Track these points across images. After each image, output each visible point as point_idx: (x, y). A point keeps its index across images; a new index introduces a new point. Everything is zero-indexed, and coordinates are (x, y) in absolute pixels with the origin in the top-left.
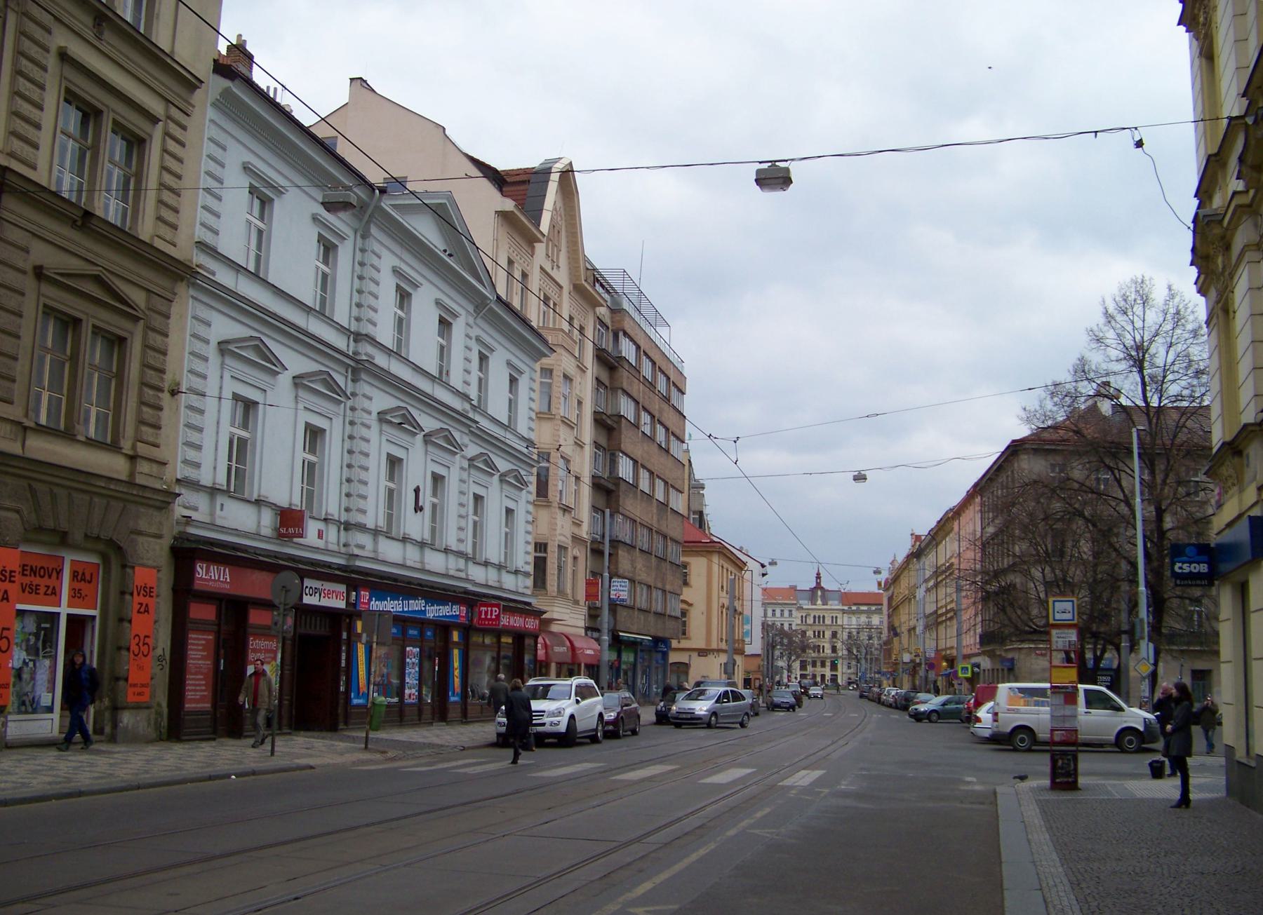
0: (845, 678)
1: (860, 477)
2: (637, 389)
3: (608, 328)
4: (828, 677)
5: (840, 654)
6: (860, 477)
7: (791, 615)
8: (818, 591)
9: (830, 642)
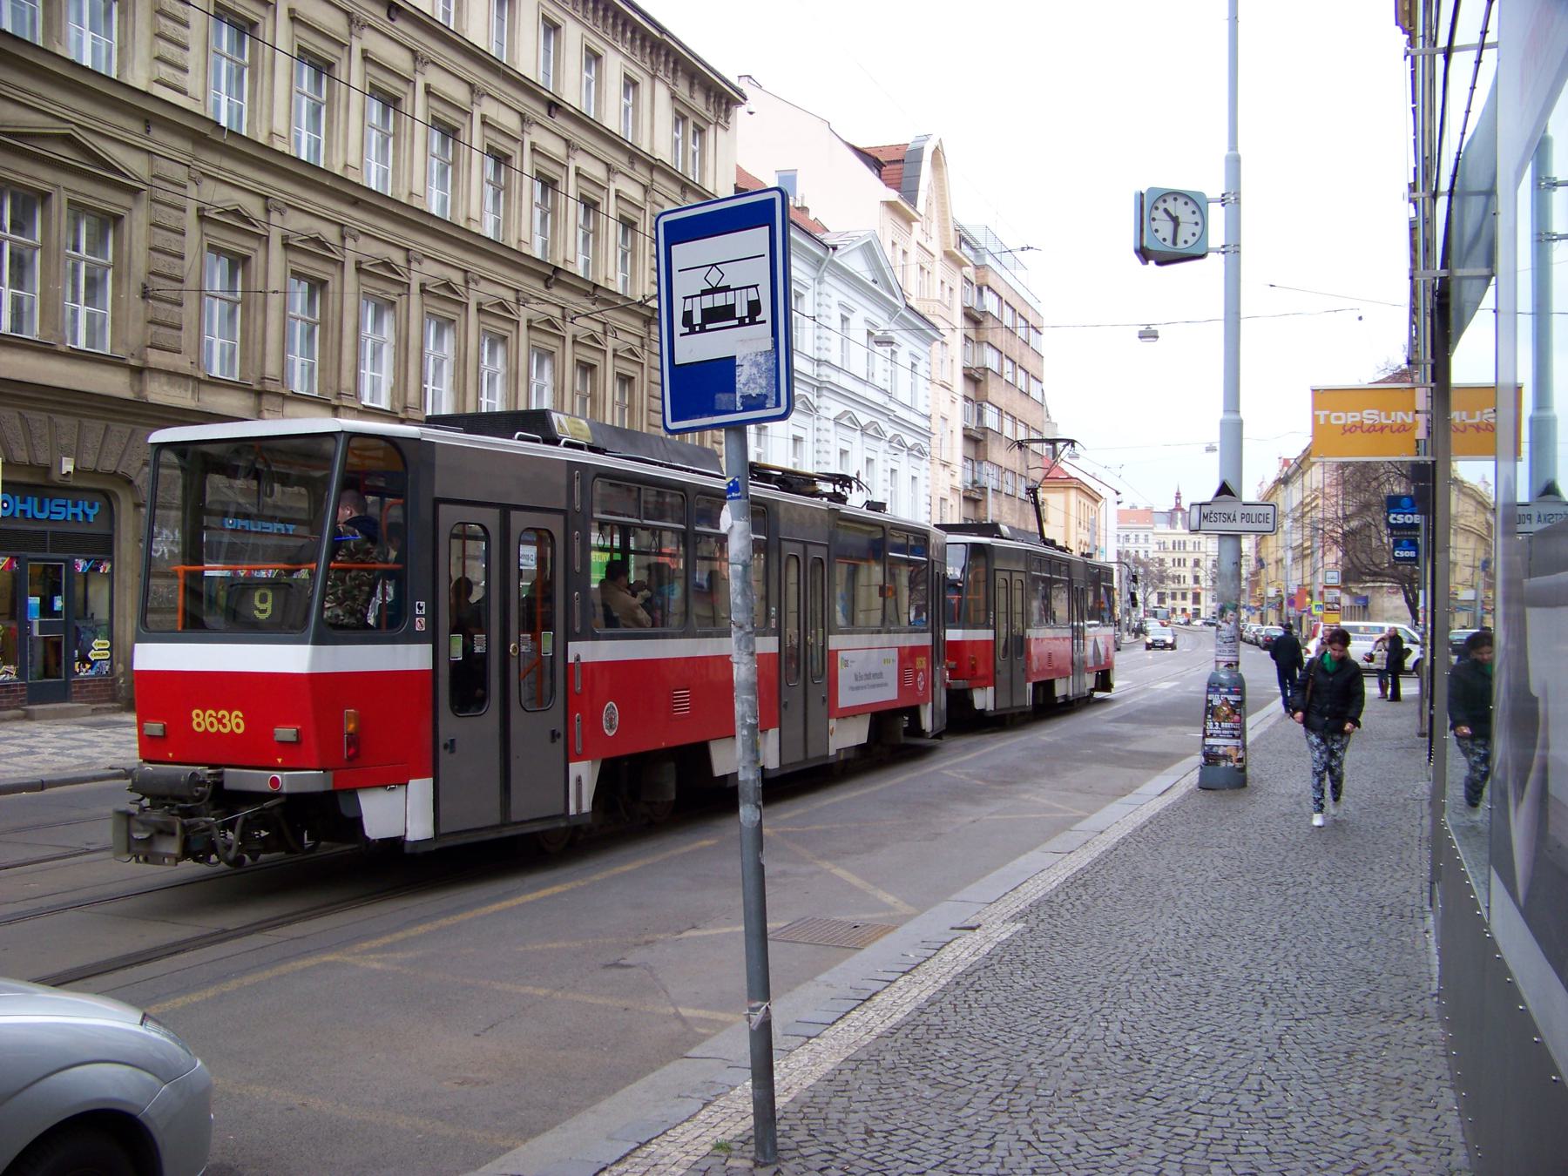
2: (1000, 338)
3: (972, 284)
5: (1203, 585)
7: (1146, 540)
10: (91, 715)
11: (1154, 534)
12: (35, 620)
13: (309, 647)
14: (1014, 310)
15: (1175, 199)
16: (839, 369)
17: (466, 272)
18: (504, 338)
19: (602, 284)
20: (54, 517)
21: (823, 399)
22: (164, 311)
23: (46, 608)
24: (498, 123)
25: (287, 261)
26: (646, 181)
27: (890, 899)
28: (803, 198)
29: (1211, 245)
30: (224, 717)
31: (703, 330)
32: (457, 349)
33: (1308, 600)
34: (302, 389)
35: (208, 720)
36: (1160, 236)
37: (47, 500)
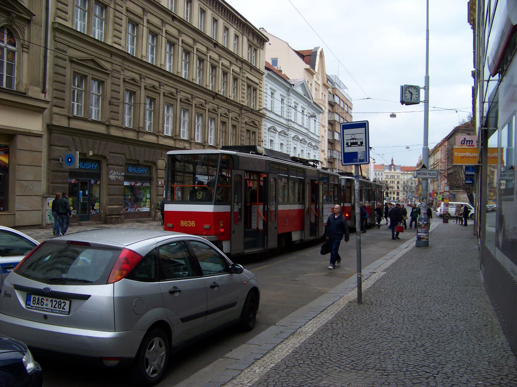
0: (402, 199)
1: (408, 148)
2: (339, 111)
3: (331, 94)
4: (396, 198)
5: (400, 190)
6: (408, 148)
7: (382, 175)
8: (392, 166)
9: (397, 185)
10: (96, 225)
11: (385, 173)
12: (81, 197)
13: (213, 206)
14: (344, 102)
15: (411, 88)
16: (294, 122)
17: (192, 95)
18: (202, 115)
19: (228, 98)
20: (86, 168)
21: (289, 132)
22: (115, 109)
23: (84, 194)
24: (201, 50)
25: (146, 93)
26: (240, 66)
27: (348, 269)
28: (280, 67)
29: (421, 100)
30: (189, 222)
31: (351, 146)
32: (189, 118)
33: (436, 195)
34: (95, 119)
35: (185, 223)
36: (407, 98)
37: (85, 163)
